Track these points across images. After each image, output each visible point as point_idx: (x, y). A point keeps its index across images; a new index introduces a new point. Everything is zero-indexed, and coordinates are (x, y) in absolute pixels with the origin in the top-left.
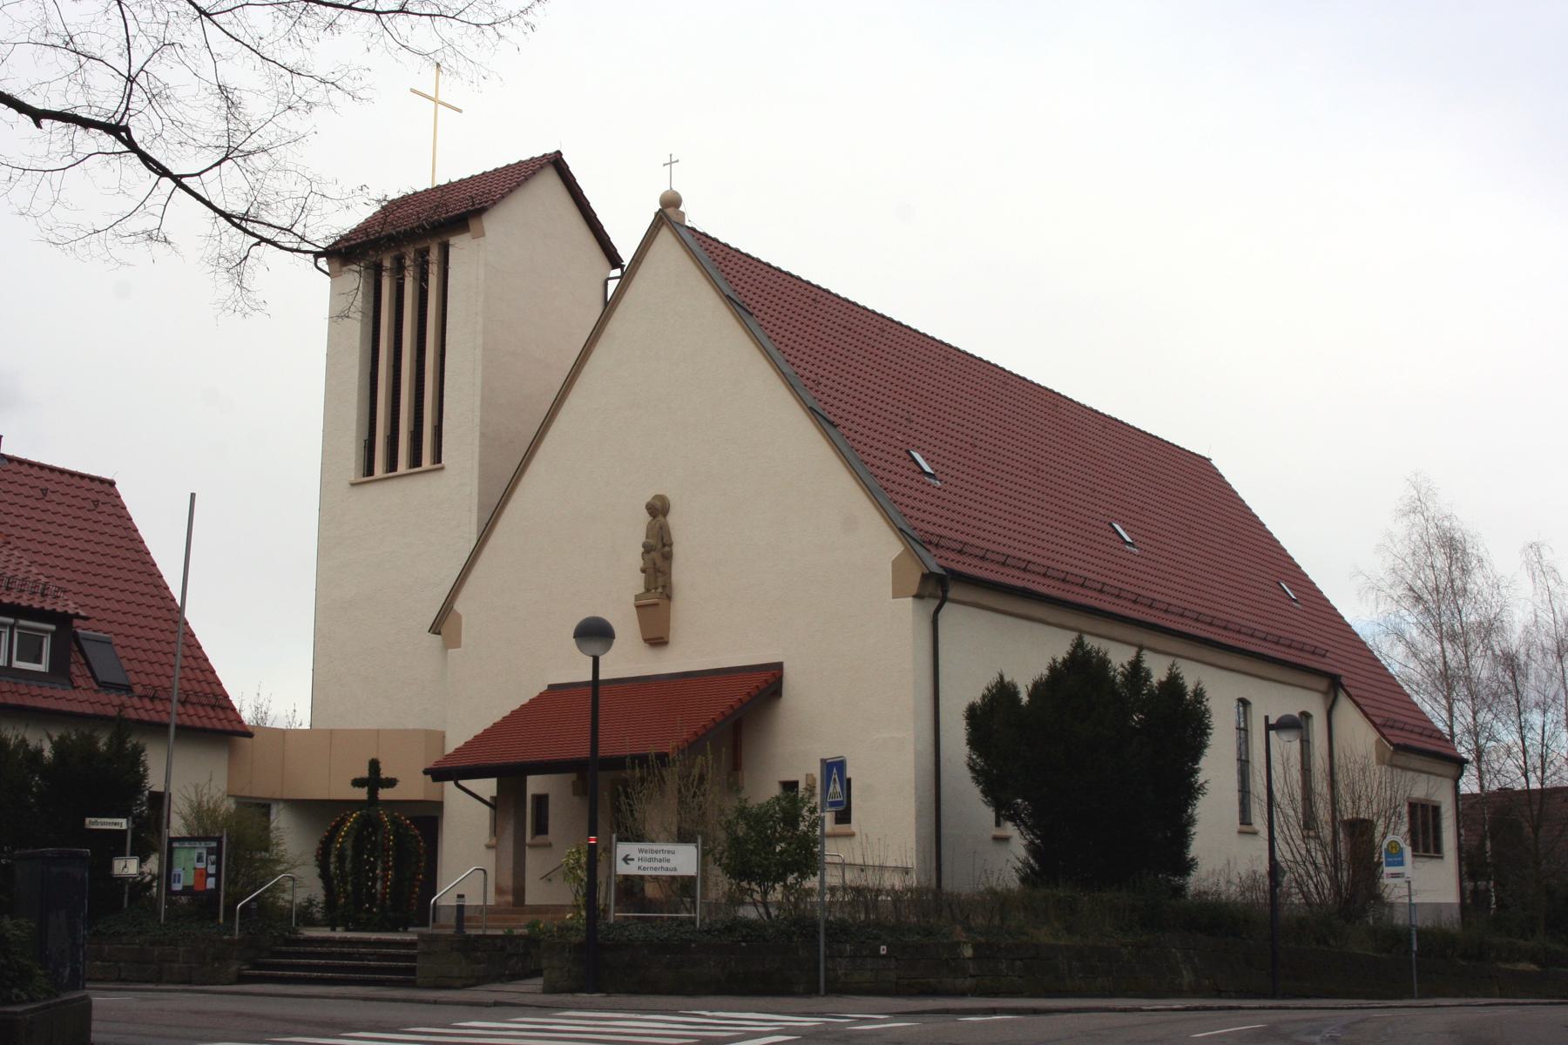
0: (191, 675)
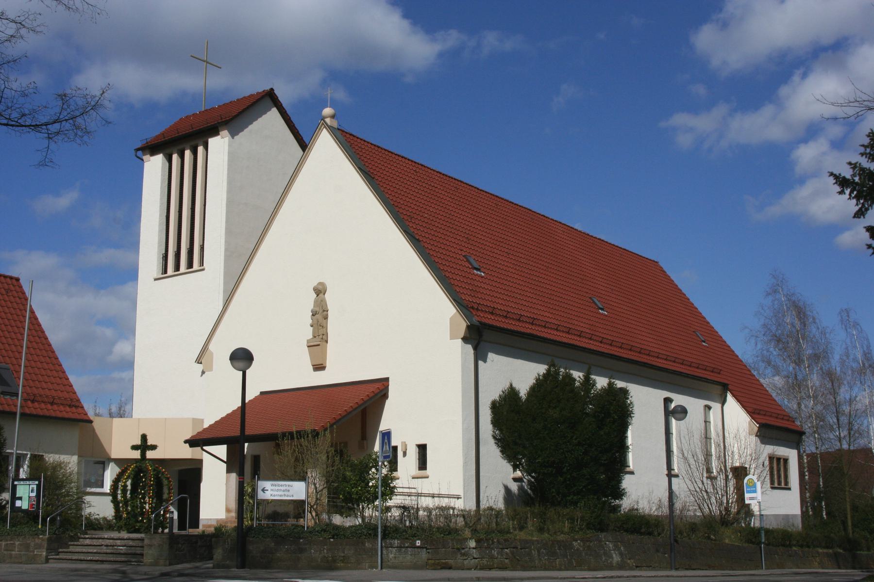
0: (32, 384)
